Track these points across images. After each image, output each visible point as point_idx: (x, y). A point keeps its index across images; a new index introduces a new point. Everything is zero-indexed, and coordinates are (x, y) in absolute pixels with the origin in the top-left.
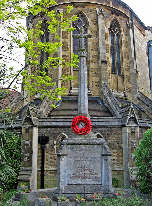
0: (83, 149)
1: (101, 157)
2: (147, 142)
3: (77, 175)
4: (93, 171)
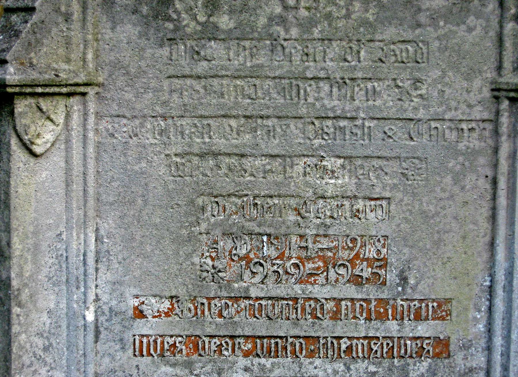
0: (282, 21)
1: (495, 121)
2: (298, 65)
3: (212, 324)
4: (391, 276)
